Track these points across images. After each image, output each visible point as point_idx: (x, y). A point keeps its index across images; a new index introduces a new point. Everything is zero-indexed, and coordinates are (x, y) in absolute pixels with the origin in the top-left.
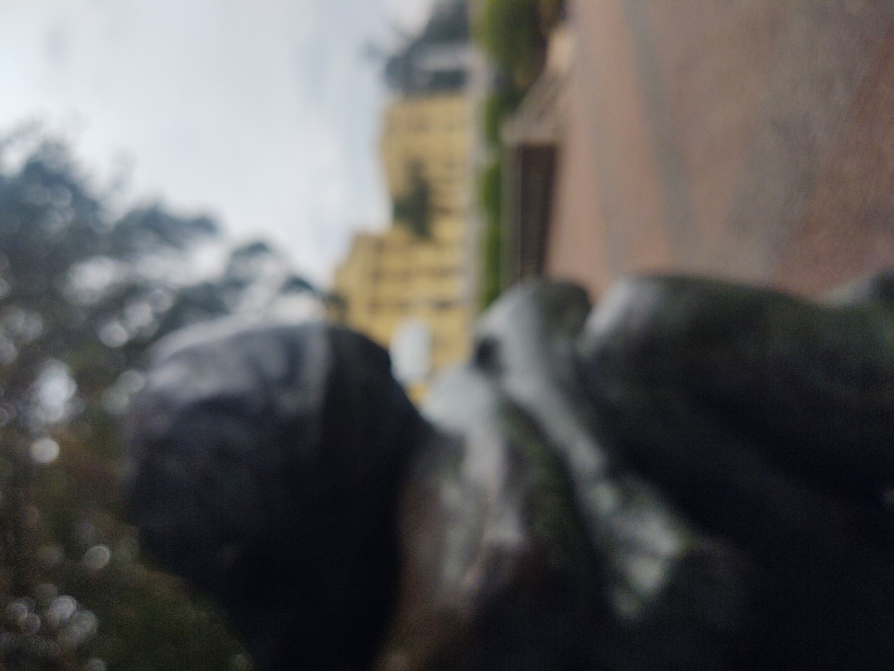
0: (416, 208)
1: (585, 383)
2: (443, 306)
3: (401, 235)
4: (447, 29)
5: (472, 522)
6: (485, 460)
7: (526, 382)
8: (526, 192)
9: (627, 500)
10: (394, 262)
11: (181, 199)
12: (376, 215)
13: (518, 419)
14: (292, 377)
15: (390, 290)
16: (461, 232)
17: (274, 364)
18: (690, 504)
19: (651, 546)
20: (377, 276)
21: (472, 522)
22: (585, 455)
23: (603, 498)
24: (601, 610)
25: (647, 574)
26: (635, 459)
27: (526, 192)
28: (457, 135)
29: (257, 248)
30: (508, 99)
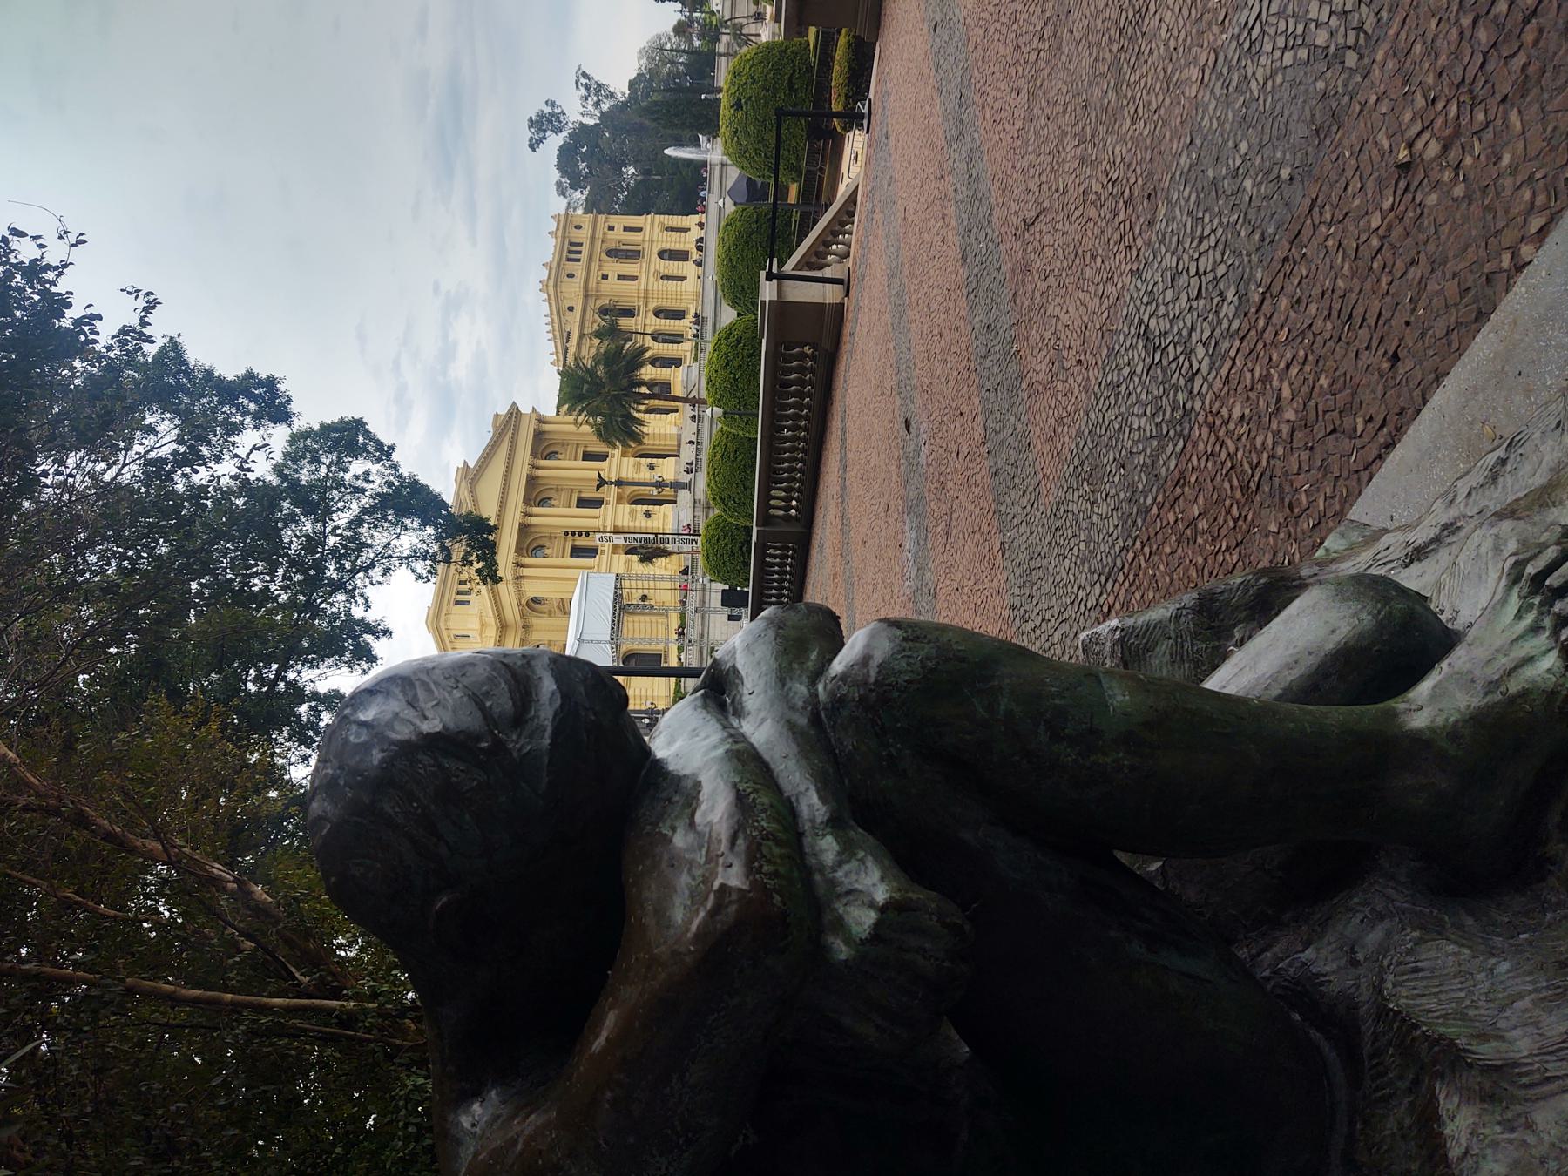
0: (608, 387)
1: (818, 730)
2: (649, 550)
3: (580, 429)
4: (673, 98)
5: (702, 859)
6: (715, 807)
7: (760, 730)
8: (785, 380)
9: (848, 850)
10: (570, 470)
11: (218, 352)
12: (541, 393)
13: (747, 762)
14: (521, 716)
15: (558, 517)
16: (679, 434)
17: (503, 703)
18: (908, 853)
19: (867, 888)
20: (536, 493)
21: (702, 859)
22: (812, 805)
23: (828, 847)
24: (819, 951)
25: (862, 920)
26: (862, 811)
27: (785, 380)
28: (679, 275)
29: (348, 437)
30: (764, 236)
